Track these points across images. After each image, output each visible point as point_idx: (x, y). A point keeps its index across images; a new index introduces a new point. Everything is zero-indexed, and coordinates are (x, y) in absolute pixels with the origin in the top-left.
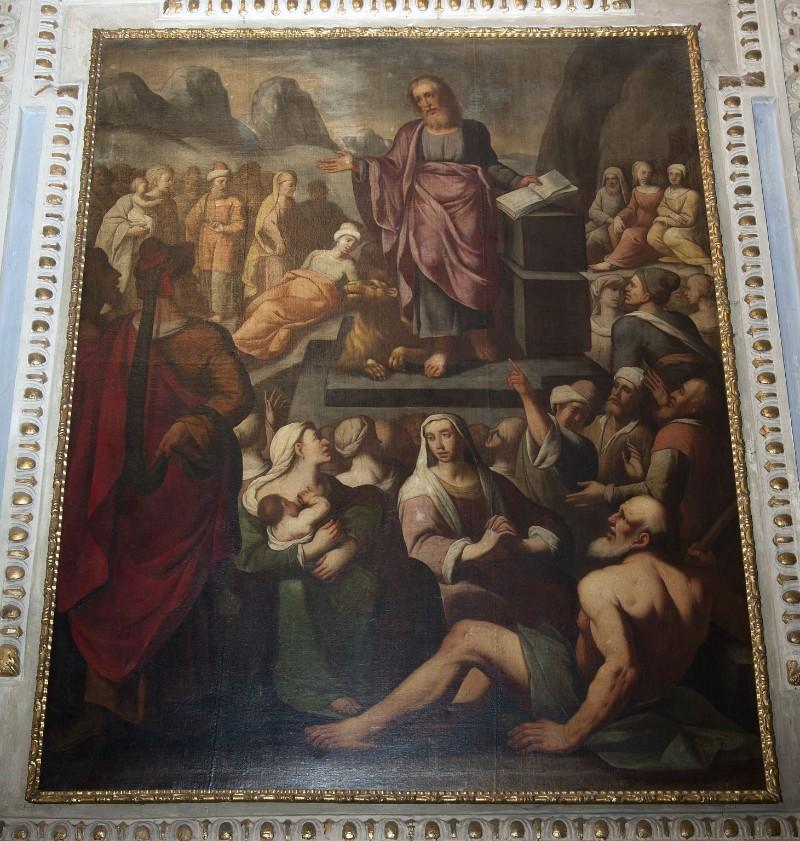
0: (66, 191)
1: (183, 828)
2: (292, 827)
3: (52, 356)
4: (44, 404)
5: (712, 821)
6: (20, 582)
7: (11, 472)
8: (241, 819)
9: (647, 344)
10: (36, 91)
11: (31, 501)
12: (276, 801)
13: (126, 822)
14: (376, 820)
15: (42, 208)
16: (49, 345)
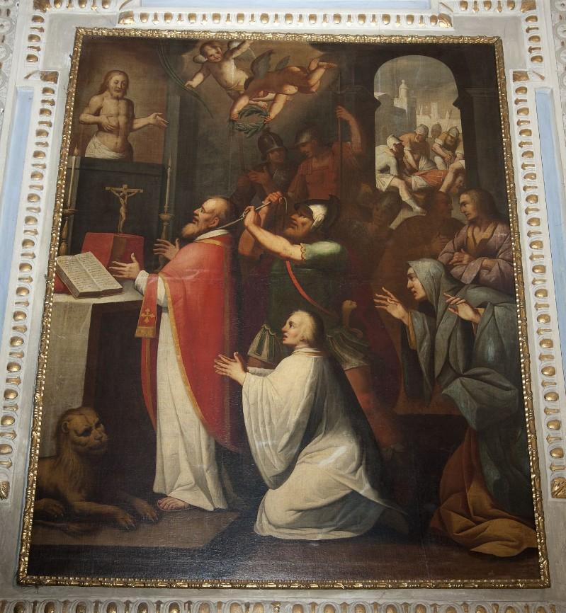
0: (37, 236)
1: (80, 607)
2: (317, 608)
3: (39, 242)
4: (31, 298)
5: (101, 603)
6: (18, 373)
7: (9, 322)
8: (63, 600)
9: (415, 292)
10: (25, 76)
11: (20, 368)
12: (188, 587)
13: (69, 599)
14: (318, 603)
15: (36, 118)
16: (34, 257)
